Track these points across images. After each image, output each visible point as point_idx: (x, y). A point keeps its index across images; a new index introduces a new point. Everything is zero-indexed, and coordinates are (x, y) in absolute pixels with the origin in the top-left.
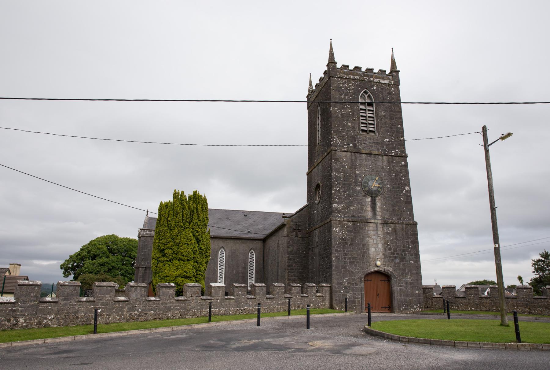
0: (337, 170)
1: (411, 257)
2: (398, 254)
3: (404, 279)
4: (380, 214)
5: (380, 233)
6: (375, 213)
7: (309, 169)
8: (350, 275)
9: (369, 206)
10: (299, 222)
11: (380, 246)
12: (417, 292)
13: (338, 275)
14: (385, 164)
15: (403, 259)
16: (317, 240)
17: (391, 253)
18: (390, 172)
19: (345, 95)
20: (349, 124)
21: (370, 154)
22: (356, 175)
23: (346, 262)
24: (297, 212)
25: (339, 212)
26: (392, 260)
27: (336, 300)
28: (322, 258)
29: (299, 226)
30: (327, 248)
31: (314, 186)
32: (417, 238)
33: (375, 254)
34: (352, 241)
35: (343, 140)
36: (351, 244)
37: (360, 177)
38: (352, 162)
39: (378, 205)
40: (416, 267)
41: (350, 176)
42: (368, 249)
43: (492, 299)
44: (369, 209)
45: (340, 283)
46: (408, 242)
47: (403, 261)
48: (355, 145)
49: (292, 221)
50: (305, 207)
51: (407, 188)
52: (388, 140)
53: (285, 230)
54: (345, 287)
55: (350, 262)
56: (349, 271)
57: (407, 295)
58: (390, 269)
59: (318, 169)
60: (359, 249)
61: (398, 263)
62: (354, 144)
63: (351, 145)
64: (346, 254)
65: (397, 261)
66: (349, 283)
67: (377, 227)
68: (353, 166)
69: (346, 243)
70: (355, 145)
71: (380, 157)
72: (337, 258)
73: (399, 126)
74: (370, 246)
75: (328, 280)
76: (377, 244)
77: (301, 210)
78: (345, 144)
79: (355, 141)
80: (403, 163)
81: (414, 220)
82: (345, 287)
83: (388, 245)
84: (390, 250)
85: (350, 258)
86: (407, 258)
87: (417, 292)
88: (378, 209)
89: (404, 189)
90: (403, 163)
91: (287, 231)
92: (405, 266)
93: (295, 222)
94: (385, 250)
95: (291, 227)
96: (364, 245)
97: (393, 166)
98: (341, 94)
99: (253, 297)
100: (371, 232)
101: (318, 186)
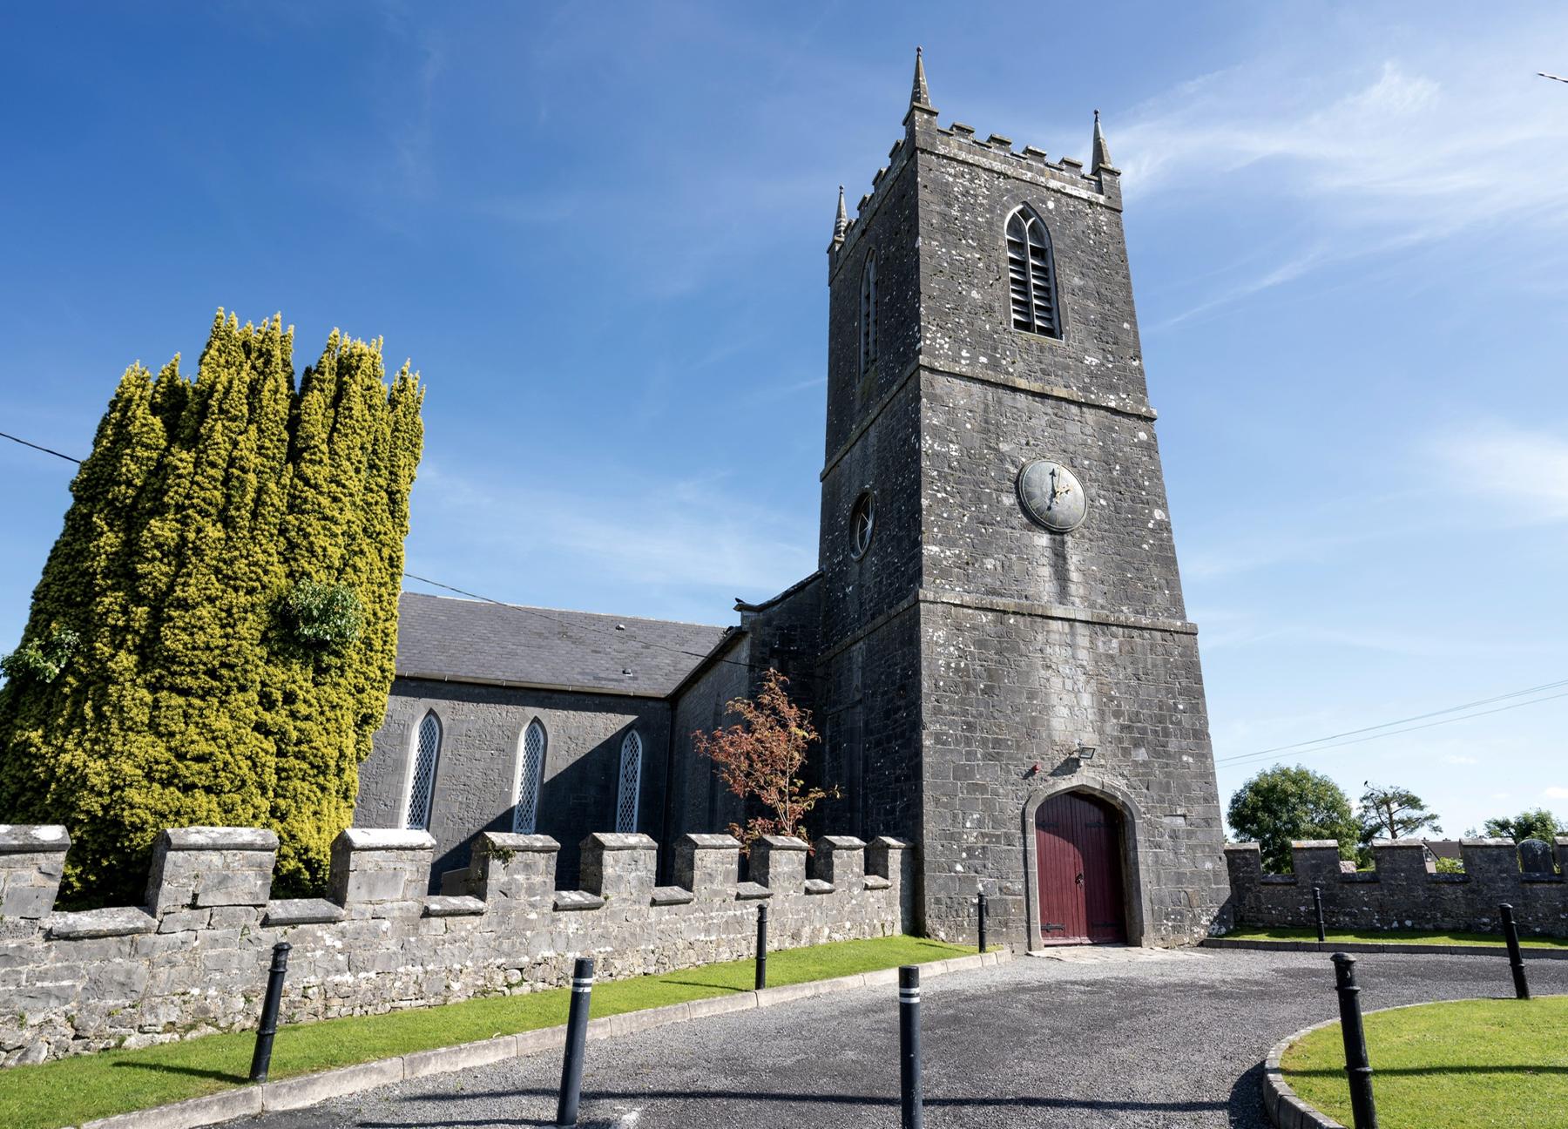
0: (937, 433)
1: (1184, 743)
2: (1143, 731)
3: (1166, 820)
4: (1081, 591)
5: (1083, 655)
6: (1065, 590)
7: (827, 461)
8: (988, 806)
9: (1044, 561)
10: (792, 628)
11: (1086, 700)
12: (1208, 865)
13: (945, 806)
14: (1089, 430)
15: (1159, 750)
16: (857, 680)
17: (1123, 728)
18: (1107, 462)
19: (963, 210)
20: (974, 294)
21: (1043, 396)
22: (1002, 457)
23: (970, 755)
24: (787, 594)
25: (945, 573)
26: (1126, 752)
27: (938, 901)
28: (878, 743)
29: (792, 641)
30: (902, 703)
31: (847, 507)
32: (1199, 680)
33: (1071, 728)
34: (990, 677)
35: (958, 342)
36: (988, 691)
37: (1013, 463)
38: (986, 410)
39: (1074, 560)
40: (1202, 776)
41: (983, 457)
42: (1047, 708)
43: (1473, 885)
44: (1046, 571)
45: (952, 837)
46: (1169, 691)
47: (1158, 755)
48: (994, 365)
49: (768, 623)
50: (814, 578)
51: (1158, 514)
52: (1095, 361)
53: (743, 652)
54: (969, 850)
55: (986, 757)
56: (983, 789)
57: (1179, 878)
58: (1121, 783)
59: (865, 448)
60: (1017, 710)
61: (1145, 764)
62: (991, 357)
63: (983, 360)
64: (971, 727)
65: (1141, 755)
66: (983, 835)
67: (1073, 634)
68: (990, 429)
69: (969, 687)
70: (994, 365)
71: (1074, 409)
72: (938, 738)
73: (1126, 325)
74: (1054, 700)
75: (909, 827)
76: (1076, 693)
77: (801, 587)
78: (964, 353)
79: (995, 349)
80: (1143, 436)
81: (1183, 617)
82: (969, 850)
83: (1112, 699)
84: (1117, 714)
85: (984, 742)
86: (1173, 745)
87: (1208, 865)
88: (1074, 576)
89: (1151, 516)
90: (1143, 436)
91: (752, 657)
92: (1168, 775)
93: (779, 628)
94: (1102, 713)
95: (764, 644)
96: (1032, 695)
97: (1114, 441)
98: (949, 205)
99: (1315, 940)
100: (1057, 653)
101: (861, 505)
